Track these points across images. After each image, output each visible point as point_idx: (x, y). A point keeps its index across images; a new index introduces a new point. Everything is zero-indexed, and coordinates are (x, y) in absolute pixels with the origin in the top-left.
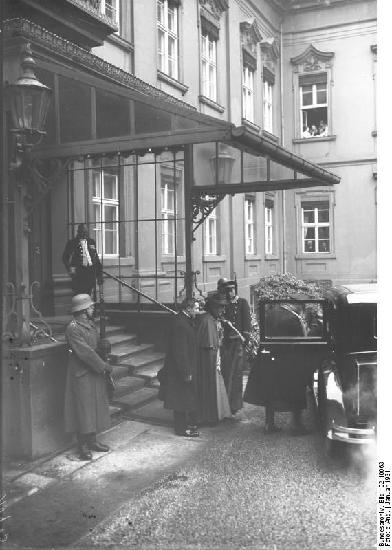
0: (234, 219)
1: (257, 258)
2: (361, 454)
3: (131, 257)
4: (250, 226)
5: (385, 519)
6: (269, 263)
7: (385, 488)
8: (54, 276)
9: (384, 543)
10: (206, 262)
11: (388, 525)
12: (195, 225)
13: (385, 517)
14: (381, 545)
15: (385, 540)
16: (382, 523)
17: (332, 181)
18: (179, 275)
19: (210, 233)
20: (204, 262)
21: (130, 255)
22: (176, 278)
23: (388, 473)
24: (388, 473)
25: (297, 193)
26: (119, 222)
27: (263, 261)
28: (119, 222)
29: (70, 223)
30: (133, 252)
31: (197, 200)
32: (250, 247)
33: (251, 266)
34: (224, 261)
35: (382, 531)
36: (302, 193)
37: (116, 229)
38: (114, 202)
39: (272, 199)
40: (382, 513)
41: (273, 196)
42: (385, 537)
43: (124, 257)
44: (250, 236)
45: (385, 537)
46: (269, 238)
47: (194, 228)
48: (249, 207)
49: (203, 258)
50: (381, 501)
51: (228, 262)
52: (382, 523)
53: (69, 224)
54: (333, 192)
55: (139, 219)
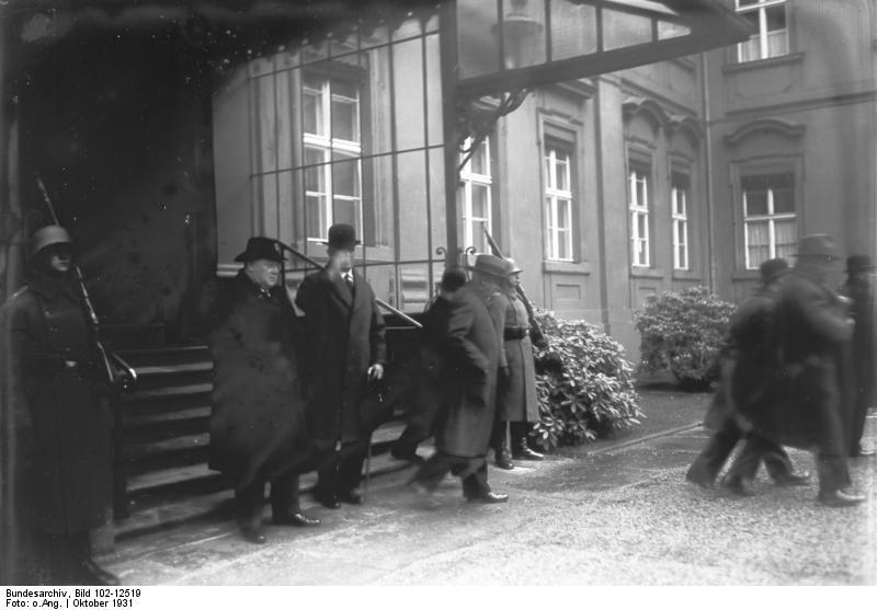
0: (606, 198)
1: (654, 273)
2: (432, 445)
3: (386, 248)
4: (641, 217)
5: (49, 599)
6: (639, 283)
7: (104, 599)
8: (220, 266)
9: (11, 597)
10: (550, 273)
11: (40, 603)
12: (729, 366)
13: (53, 599)
14: (9, 593)
15: (15, 599)
16: (43, 594)
17: (796, 135)
18: (435, 257)
19: (681, 240)
20: (546, 272)
21: (385, 243)
22: (430, 262)
23: (129, 603)
24: (129, 603)
25: (734, 162)
26: (332, 163)
27: (668, 281)
28: (332, 163)
29: (255, 172)
30: (390, 236)
31: (468, 114)
32: (642, 255)
33: (641, 288)
34: (587, 274)
35: (31, 594)
36: (743, 161)
37: (324, 191)
38: (352, 147)
39: (686, 171)
40: (59, 595)
41: (688, 167)
42: (21, 599)
43: (373, 245)
44: (641, 234)
45: (21, 599)
46: (679, 242)
47: (461, 161)
48: (639, 186)
49: (544, 264)
50: (77, 593)
51: (596, 278)
52: (43, 594)
53: (252, 176)
54: (801, 155)
55: (402, 259)
